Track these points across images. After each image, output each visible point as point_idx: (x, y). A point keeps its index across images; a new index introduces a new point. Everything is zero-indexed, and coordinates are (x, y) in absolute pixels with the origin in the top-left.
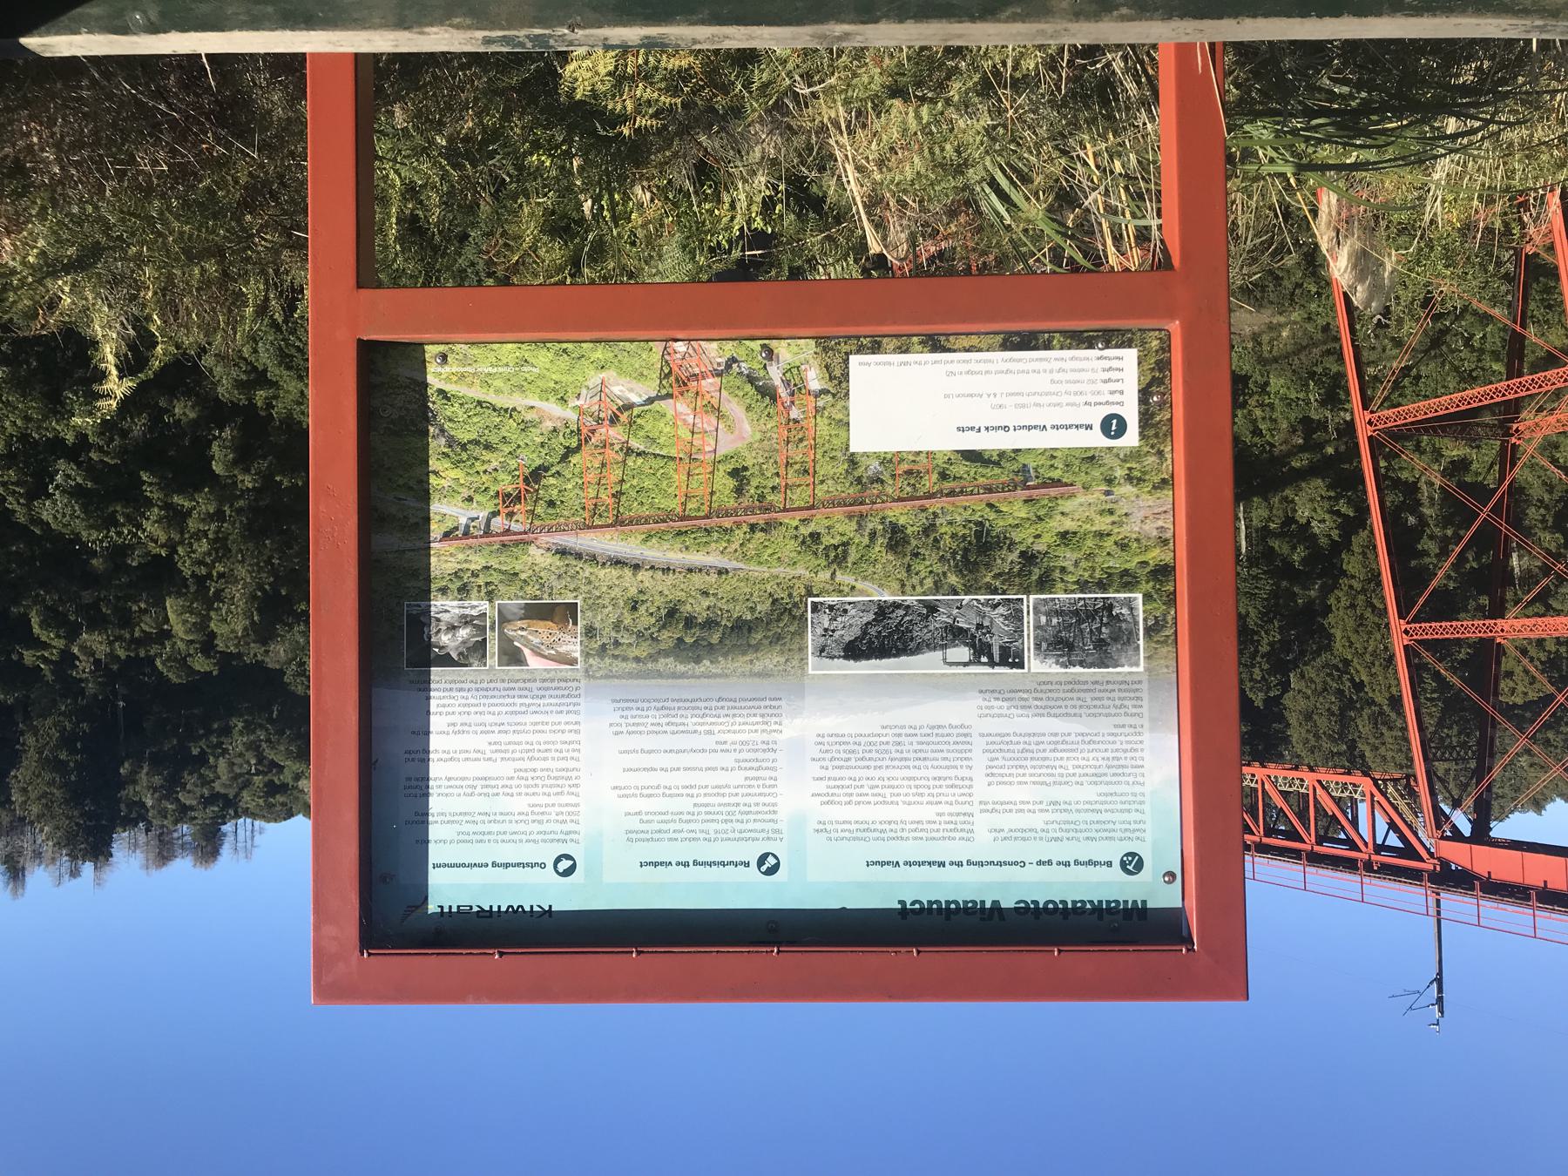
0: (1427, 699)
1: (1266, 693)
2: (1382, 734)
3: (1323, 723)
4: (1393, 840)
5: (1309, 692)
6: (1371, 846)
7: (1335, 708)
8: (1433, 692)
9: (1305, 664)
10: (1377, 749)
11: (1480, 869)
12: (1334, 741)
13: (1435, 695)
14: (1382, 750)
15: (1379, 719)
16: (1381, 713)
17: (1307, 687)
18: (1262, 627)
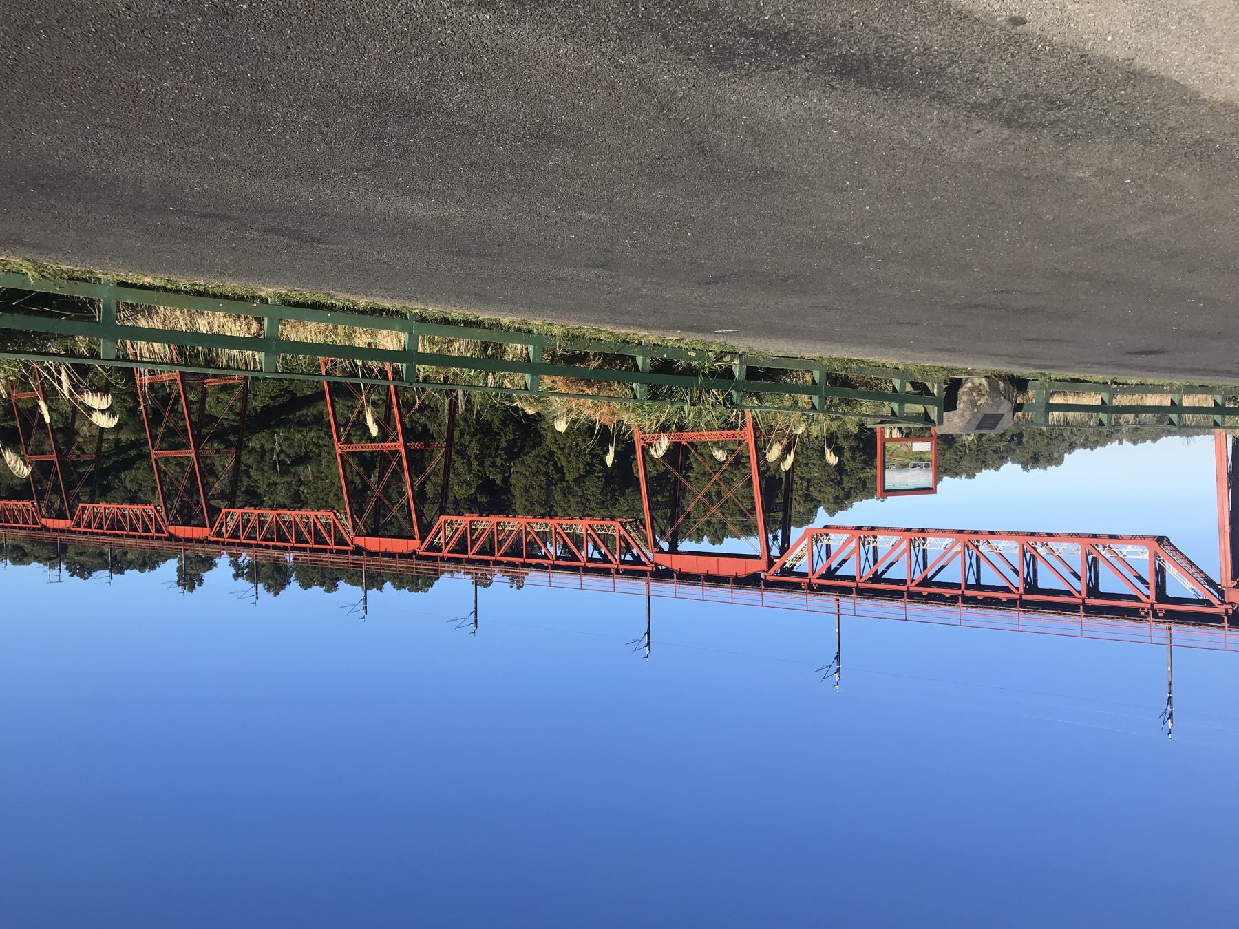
0: (596, 477)
1: (503, 475)
2: (569, 500)
3: (535, 493)
4: (596, 555)
5: (527, 474)
6: (618, 560)
7: (543, 484)
8: (600, 472)
9: (525, 455)
10: (565, 510)
11: (676, 567)
12: (542, 506)
13: (601, 474)
14: (569, 511)
15: (567, 491)
16: (569, 487)
17: (526, 470)
18: (502, 430)
